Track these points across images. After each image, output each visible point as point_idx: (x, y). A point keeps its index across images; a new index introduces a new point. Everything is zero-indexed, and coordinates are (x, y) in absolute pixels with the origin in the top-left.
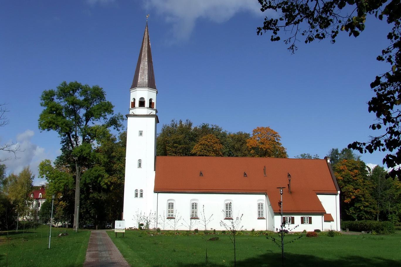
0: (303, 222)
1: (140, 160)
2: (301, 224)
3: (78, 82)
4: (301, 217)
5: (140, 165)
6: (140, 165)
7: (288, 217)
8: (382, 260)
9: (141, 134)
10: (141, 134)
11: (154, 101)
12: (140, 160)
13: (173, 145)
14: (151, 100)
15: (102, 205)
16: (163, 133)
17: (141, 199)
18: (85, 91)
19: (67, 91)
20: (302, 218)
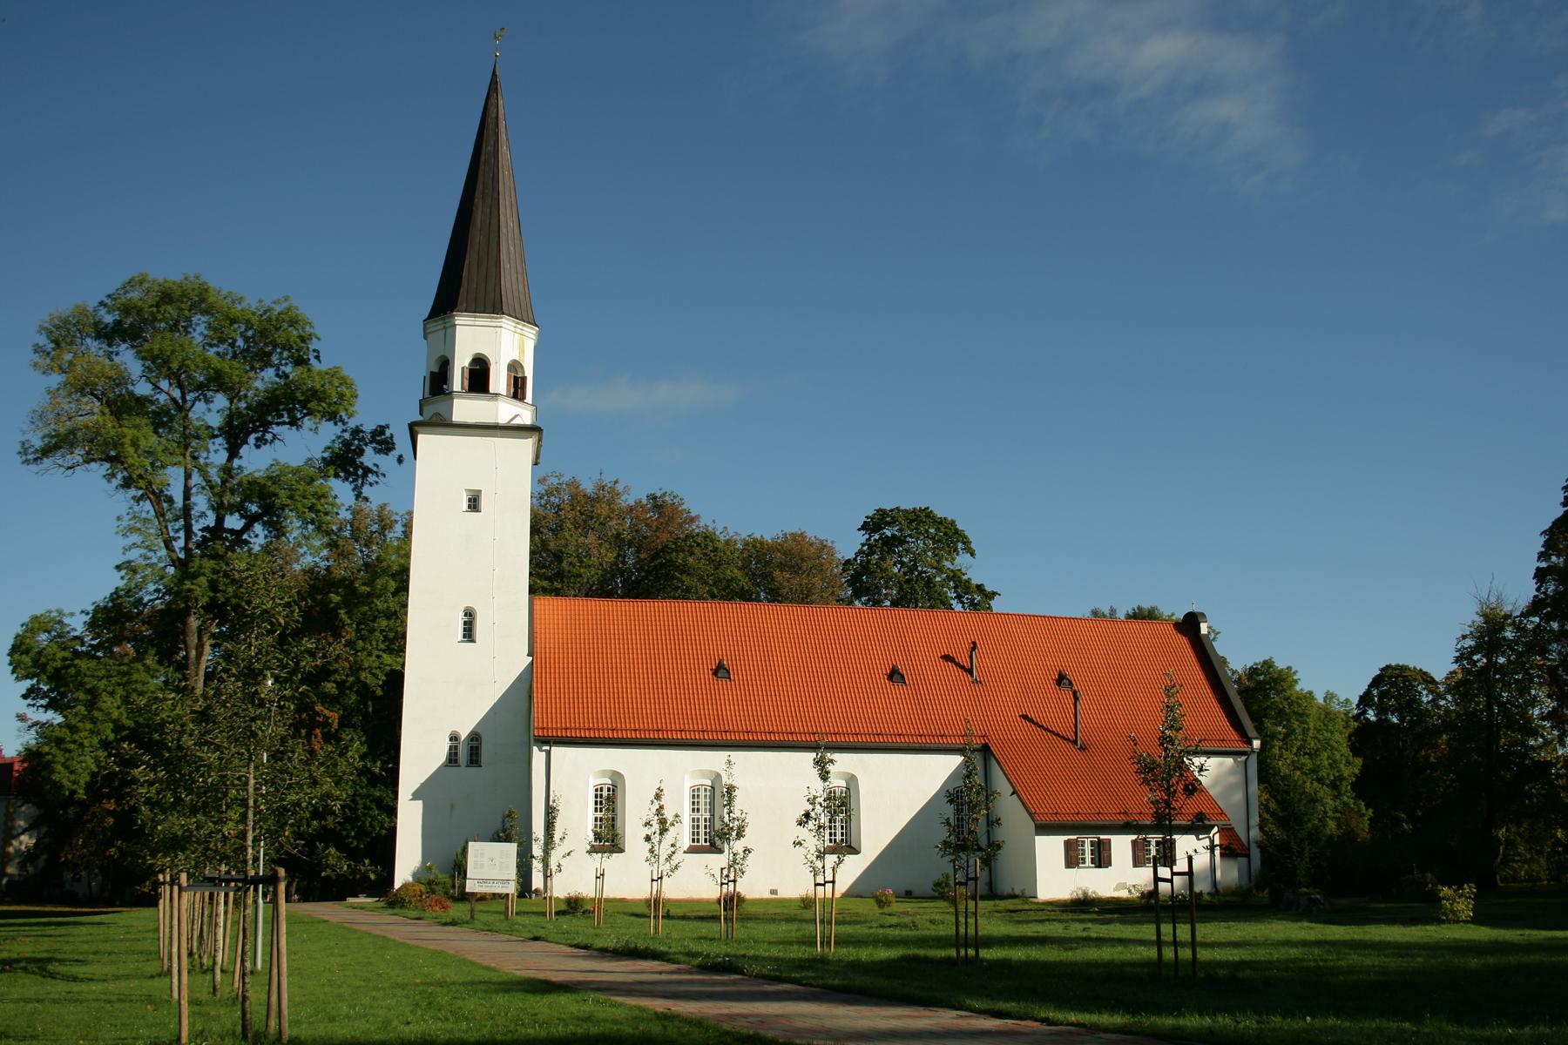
0: (1072, 860)
1: (470, 614)
2: (1135, 865)
3: (203, 279)
4: (1067, 843)
5: (469, 633)
6: (469, 633)
7: (1087, 842)
8: (1043, 1015)
9: (474, 504)
10: (474, 504)
11: (529, 372)
12: (470, 614)
13: (594, 553)
14: (514, 367)
15: (111, 820)
16: (593, 500)
17: (474, 770)
18: (224, 322)
19: (136, 320)
20: (1068, 845)
